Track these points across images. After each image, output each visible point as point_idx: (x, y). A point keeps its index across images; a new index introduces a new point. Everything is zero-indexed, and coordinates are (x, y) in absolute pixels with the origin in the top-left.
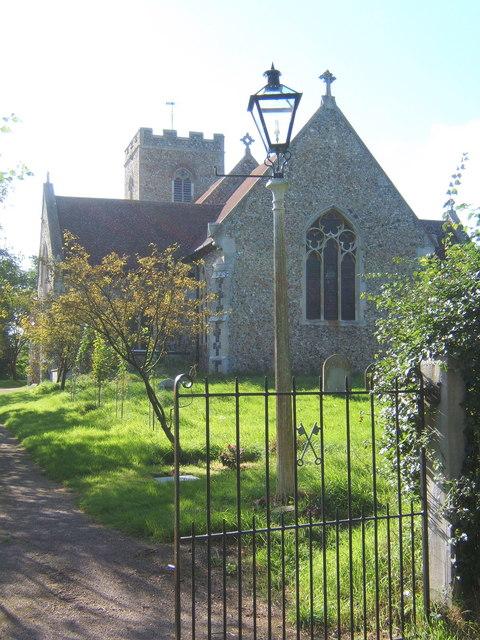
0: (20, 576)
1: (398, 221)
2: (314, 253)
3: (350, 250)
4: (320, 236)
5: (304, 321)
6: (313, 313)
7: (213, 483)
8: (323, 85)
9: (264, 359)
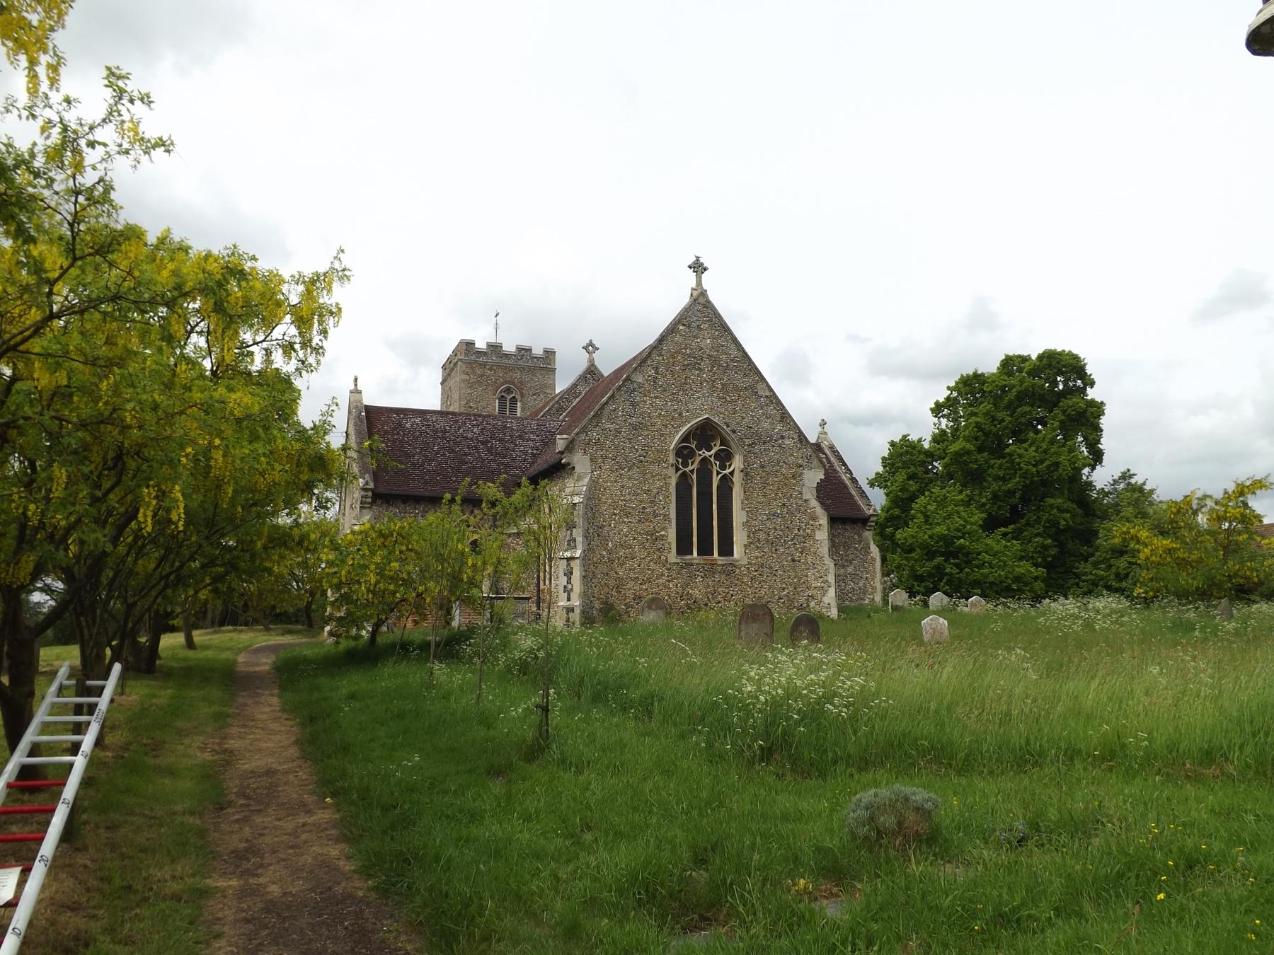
1: (783, 437)
2: (684, 475)
3: (727, 471)
4: (692, 454)
5: (673, 557)
7: (382, 490)
8: (691, 277)
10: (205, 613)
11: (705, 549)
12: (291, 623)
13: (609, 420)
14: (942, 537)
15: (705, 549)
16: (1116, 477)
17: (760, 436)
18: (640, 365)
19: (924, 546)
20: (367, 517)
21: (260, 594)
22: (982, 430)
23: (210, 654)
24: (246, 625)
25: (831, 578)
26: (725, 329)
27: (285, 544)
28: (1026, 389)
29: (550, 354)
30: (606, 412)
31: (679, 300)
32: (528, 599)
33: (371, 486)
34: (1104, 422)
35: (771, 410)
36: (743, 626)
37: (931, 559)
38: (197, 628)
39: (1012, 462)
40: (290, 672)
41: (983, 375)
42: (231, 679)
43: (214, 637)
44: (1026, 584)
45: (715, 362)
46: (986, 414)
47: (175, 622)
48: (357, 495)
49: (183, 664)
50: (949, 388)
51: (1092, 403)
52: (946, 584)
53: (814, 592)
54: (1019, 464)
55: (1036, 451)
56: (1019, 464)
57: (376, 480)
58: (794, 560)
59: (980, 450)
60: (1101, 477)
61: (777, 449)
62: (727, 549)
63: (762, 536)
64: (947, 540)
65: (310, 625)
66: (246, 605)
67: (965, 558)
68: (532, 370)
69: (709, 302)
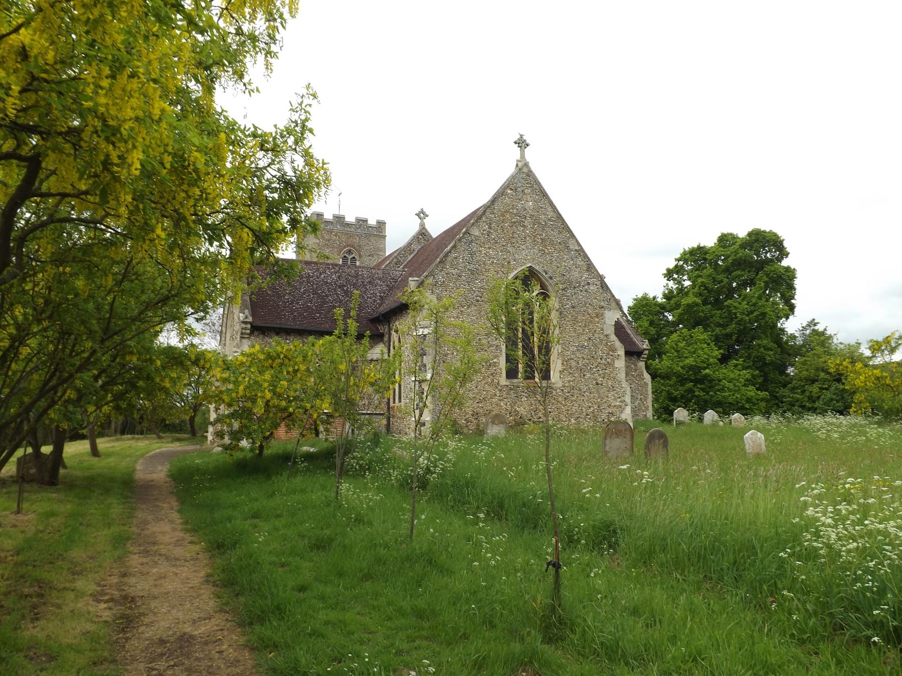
0: (158, 328)
1: (588, 284)
5: (503, 381)
6: (512, 374)
7: (259, 323)
9: (466, 420)
10: (110, 423)
11: (529, 376)
12: (177, 432)
13: (452, 266)
14: (691, 368)
15: (529, 376)
16: (804, 325)
17: (571, 283)
18: (477, 221)
19: (678, 375)
20: (246, 347)
21: (154, 409)
22: (706, 288)
23: (111, 461)
24: (142, 434)
25: (628, 399)
26: (544, 195)
27: (181, 364)
28: (741, 258)
29: (381, 225)
30: (449, 259)
31: (507, 170)
32: (381, 414)
33: (250, 319)
34: (797, 283)
35: (580, 261)
36: (608, 442)
37: (683, 385)
38: (101, 435)
39: (730, 312)
40: (187, 482)
41: (704, 247)
42: (129, 488)
43: (116, 444)
44: (754, 404)
45: (536, 221)
46: (709, 276)
47: (85, 432)
48: (237, 327)
49: (87, 474)
50: (676, 260)
51: (788, 269)
52: (695, 403)
53: (614, 410)
54: (735, 314)
55: (748, 304)
56: (735, 314)
57: (253, 315)
58: (597, 384)
59: (705, 303)
60: (792, 326)
61: (584, 293)
62: (546, 376)
63: (573, 364)
64: (695, 369)
65: (193, 433)
66: (141, 418)
67: (708, 383)
68: (368, 236)
69: (531, 171)
